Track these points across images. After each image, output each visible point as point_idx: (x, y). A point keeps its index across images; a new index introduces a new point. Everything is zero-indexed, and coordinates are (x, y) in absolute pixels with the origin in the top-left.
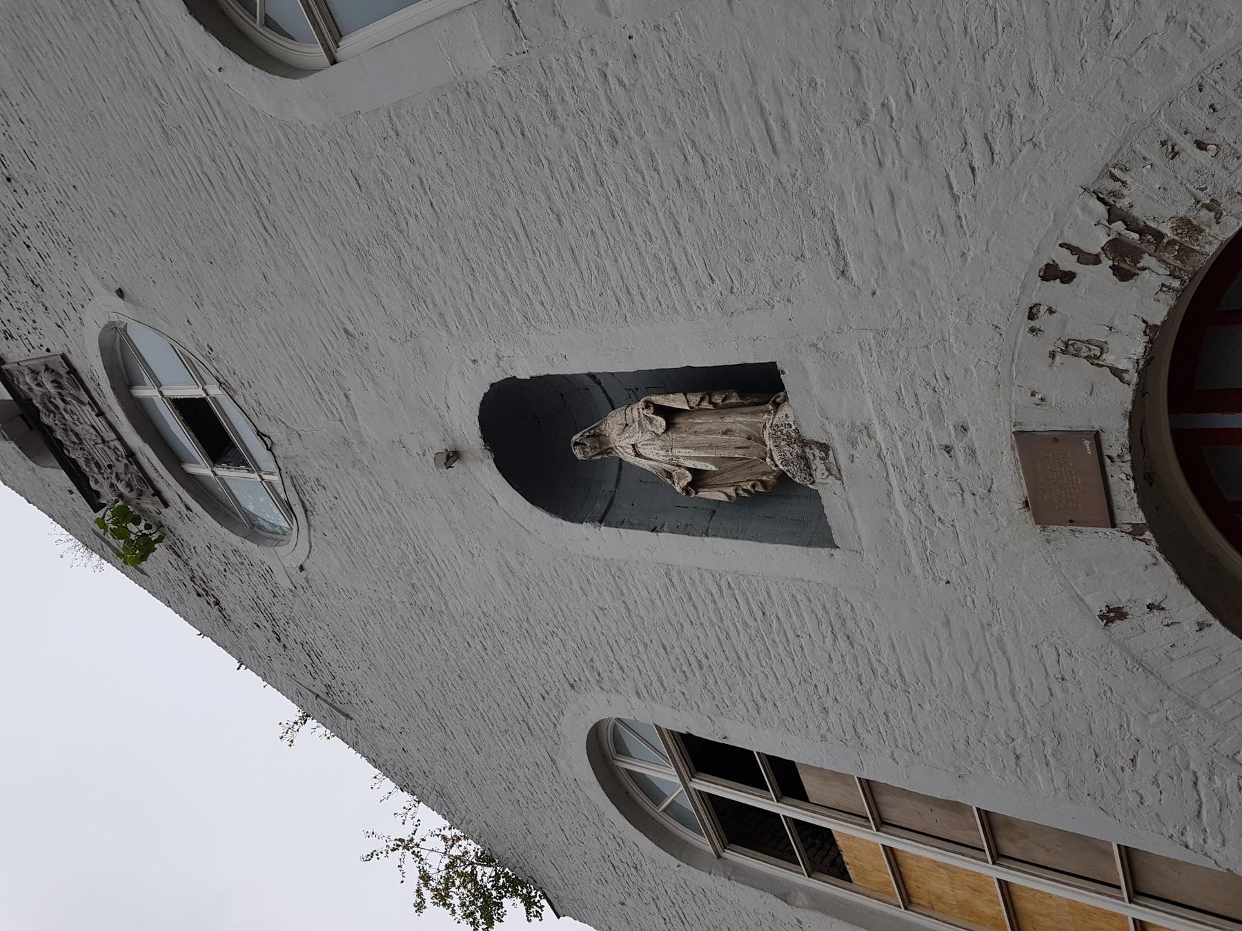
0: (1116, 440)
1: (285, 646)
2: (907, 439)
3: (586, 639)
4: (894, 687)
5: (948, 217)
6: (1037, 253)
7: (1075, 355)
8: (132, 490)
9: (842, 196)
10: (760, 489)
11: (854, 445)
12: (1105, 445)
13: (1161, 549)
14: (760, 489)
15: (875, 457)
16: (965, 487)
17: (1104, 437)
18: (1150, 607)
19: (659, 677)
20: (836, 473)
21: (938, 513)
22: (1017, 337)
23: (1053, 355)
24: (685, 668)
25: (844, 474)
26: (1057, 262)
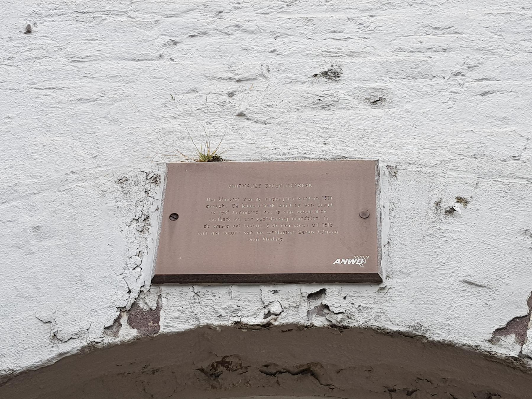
0: (349, 305)
2: (352, 27)
12: (348, 290)
13: (91, 352)
16: (246, 85)
21: (187, 43)
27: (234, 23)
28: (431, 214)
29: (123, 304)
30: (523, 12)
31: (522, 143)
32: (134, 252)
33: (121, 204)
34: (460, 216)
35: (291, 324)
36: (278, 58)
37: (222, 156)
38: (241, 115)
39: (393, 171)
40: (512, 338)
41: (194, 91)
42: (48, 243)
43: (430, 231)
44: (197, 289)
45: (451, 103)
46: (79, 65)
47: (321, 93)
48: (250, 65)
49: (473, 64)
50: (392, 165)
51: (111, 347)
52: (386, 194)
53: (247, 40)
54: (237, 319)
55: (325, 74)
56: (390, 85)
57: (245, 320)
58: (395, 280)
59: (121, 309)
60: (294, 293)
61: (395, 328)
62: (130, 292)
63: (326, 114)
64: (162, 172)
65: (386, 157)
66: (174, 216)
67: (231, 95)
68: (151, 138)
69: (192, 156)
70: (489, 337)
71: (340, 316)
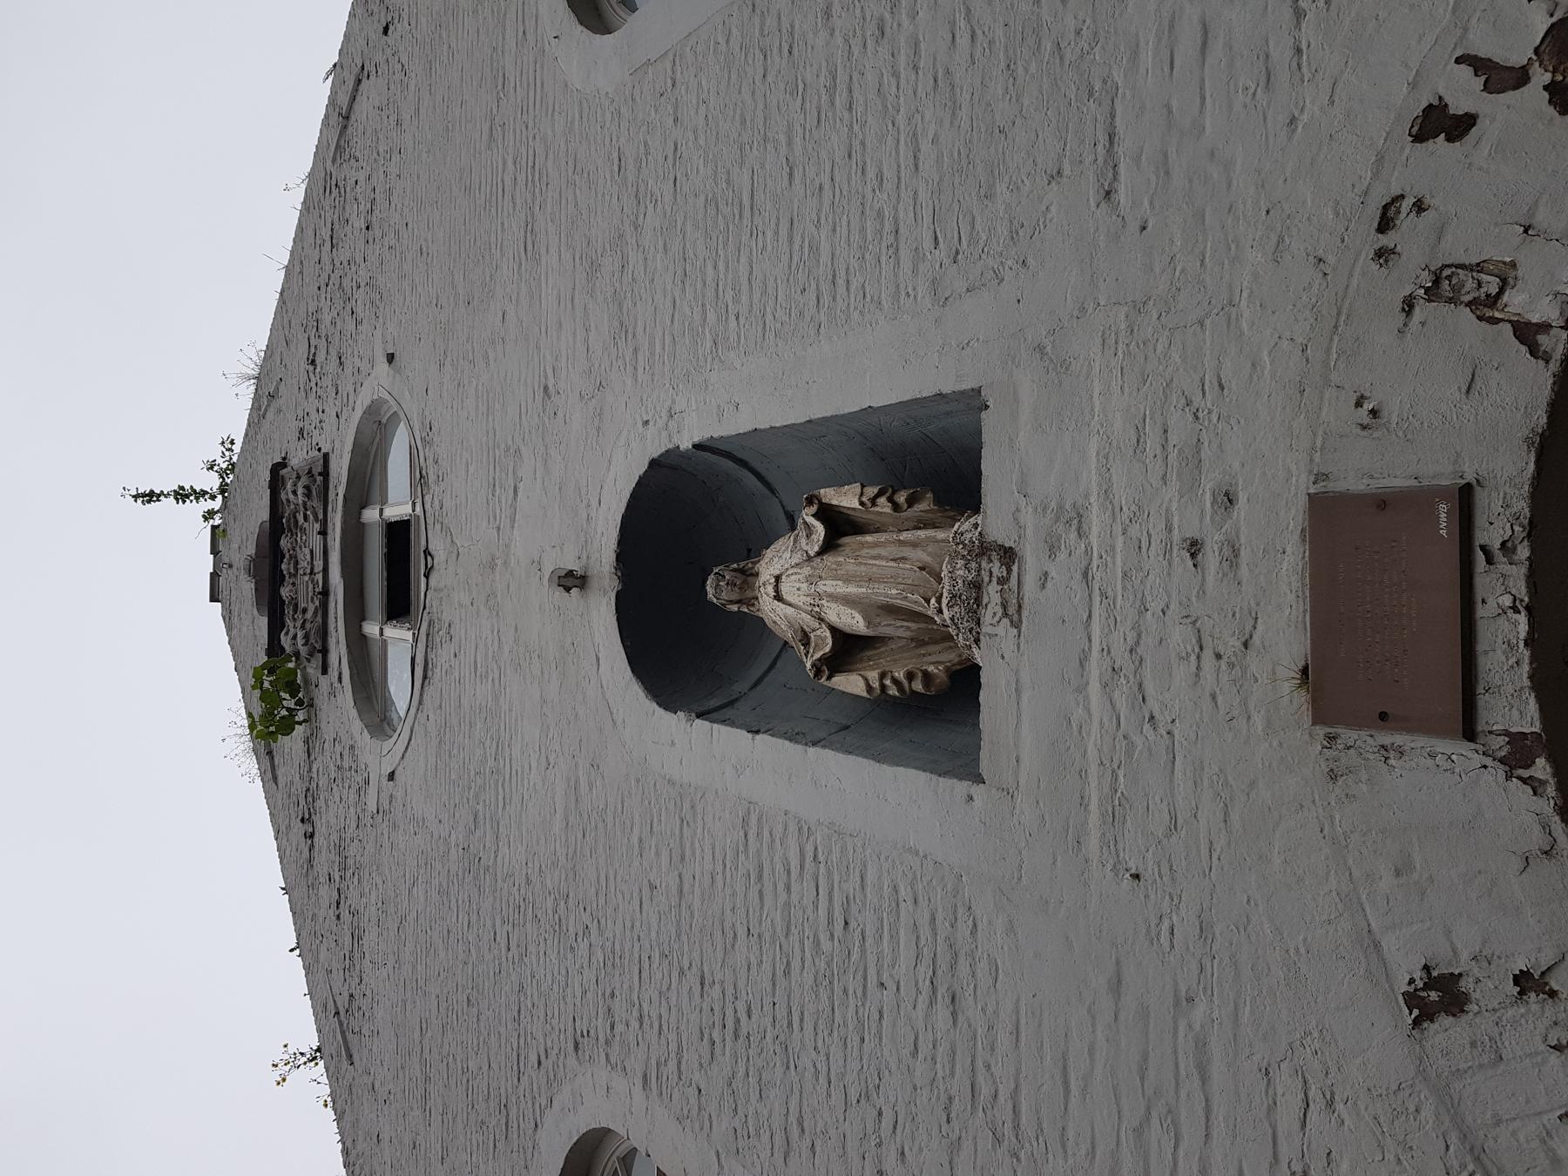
1: (338, 917)
2: (1134, 531)
3: (617, 947)
4: (998, 1140)
5: (1281, 54)
6: (1413, 85)
7: (1450, 301)
8: (305, 644)
9: (1135, 53)
10: (918, 686)
11: (1052, 551)
12: (1480, 520)
14: (918, 686)
15: (1078, 576)
16: (1207, 640)
17: (1481, 498)
18: (1524, 981)
19: (680, 1046)
20: (1013, 614)
21: (1153, 705)
22: (1351, 275)
23: (1408, 305)
24: (716, 1035)
25: (1025, 613)
26: (1447, 99)
27: (1127, 655)
28: (1375, 435)
29: (1501, 774)
30: (1120, 354)
31: (1285, 344)
32: (1430, 762)
33: (1364, 777)
34: (1380, 403)
35: (1527, 582)
36: (1172, 607)
37: (1301, 664)
38: (1246, 645)
39: (1321, 477)
40: (1541, 338)
41: (1214, 697)
42: (1417, 860)
43: (1401, 434)
44: (1480, 690)
45: (1233, 421)
46: (1180, 821)
47: (1218, 559)
48: (1180, 637)
49: (1183, 401)
50: (1312, 478)
51: (1560, 788)
52: (1350, 481)
53: (1149, 640)
54: (1522, 644)
55: (1193, 556)
56: (1208, 487)
57: (1523, 635)
58: (1466, 468)
59: (1508, 777)
60: (1485, 581)
61: (1532, 466)
62: (1485, 767)
63: (1244, 554)
64: (1321, 731)
65: (1302, 485)
66: (1383, 716)
67: (1218, 656)
68: (1275, 744)
69: (1302, 697)
70: (1541, 362)
71: (1516, 528)
